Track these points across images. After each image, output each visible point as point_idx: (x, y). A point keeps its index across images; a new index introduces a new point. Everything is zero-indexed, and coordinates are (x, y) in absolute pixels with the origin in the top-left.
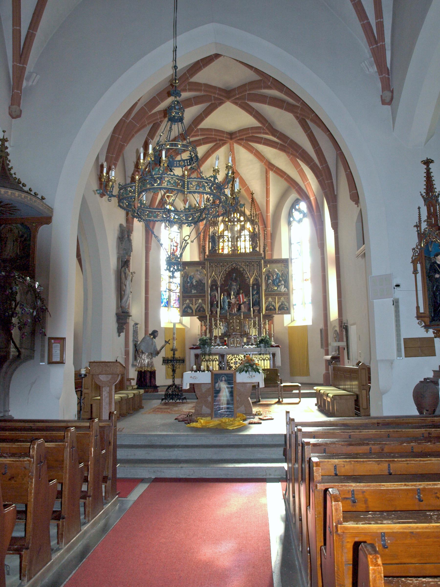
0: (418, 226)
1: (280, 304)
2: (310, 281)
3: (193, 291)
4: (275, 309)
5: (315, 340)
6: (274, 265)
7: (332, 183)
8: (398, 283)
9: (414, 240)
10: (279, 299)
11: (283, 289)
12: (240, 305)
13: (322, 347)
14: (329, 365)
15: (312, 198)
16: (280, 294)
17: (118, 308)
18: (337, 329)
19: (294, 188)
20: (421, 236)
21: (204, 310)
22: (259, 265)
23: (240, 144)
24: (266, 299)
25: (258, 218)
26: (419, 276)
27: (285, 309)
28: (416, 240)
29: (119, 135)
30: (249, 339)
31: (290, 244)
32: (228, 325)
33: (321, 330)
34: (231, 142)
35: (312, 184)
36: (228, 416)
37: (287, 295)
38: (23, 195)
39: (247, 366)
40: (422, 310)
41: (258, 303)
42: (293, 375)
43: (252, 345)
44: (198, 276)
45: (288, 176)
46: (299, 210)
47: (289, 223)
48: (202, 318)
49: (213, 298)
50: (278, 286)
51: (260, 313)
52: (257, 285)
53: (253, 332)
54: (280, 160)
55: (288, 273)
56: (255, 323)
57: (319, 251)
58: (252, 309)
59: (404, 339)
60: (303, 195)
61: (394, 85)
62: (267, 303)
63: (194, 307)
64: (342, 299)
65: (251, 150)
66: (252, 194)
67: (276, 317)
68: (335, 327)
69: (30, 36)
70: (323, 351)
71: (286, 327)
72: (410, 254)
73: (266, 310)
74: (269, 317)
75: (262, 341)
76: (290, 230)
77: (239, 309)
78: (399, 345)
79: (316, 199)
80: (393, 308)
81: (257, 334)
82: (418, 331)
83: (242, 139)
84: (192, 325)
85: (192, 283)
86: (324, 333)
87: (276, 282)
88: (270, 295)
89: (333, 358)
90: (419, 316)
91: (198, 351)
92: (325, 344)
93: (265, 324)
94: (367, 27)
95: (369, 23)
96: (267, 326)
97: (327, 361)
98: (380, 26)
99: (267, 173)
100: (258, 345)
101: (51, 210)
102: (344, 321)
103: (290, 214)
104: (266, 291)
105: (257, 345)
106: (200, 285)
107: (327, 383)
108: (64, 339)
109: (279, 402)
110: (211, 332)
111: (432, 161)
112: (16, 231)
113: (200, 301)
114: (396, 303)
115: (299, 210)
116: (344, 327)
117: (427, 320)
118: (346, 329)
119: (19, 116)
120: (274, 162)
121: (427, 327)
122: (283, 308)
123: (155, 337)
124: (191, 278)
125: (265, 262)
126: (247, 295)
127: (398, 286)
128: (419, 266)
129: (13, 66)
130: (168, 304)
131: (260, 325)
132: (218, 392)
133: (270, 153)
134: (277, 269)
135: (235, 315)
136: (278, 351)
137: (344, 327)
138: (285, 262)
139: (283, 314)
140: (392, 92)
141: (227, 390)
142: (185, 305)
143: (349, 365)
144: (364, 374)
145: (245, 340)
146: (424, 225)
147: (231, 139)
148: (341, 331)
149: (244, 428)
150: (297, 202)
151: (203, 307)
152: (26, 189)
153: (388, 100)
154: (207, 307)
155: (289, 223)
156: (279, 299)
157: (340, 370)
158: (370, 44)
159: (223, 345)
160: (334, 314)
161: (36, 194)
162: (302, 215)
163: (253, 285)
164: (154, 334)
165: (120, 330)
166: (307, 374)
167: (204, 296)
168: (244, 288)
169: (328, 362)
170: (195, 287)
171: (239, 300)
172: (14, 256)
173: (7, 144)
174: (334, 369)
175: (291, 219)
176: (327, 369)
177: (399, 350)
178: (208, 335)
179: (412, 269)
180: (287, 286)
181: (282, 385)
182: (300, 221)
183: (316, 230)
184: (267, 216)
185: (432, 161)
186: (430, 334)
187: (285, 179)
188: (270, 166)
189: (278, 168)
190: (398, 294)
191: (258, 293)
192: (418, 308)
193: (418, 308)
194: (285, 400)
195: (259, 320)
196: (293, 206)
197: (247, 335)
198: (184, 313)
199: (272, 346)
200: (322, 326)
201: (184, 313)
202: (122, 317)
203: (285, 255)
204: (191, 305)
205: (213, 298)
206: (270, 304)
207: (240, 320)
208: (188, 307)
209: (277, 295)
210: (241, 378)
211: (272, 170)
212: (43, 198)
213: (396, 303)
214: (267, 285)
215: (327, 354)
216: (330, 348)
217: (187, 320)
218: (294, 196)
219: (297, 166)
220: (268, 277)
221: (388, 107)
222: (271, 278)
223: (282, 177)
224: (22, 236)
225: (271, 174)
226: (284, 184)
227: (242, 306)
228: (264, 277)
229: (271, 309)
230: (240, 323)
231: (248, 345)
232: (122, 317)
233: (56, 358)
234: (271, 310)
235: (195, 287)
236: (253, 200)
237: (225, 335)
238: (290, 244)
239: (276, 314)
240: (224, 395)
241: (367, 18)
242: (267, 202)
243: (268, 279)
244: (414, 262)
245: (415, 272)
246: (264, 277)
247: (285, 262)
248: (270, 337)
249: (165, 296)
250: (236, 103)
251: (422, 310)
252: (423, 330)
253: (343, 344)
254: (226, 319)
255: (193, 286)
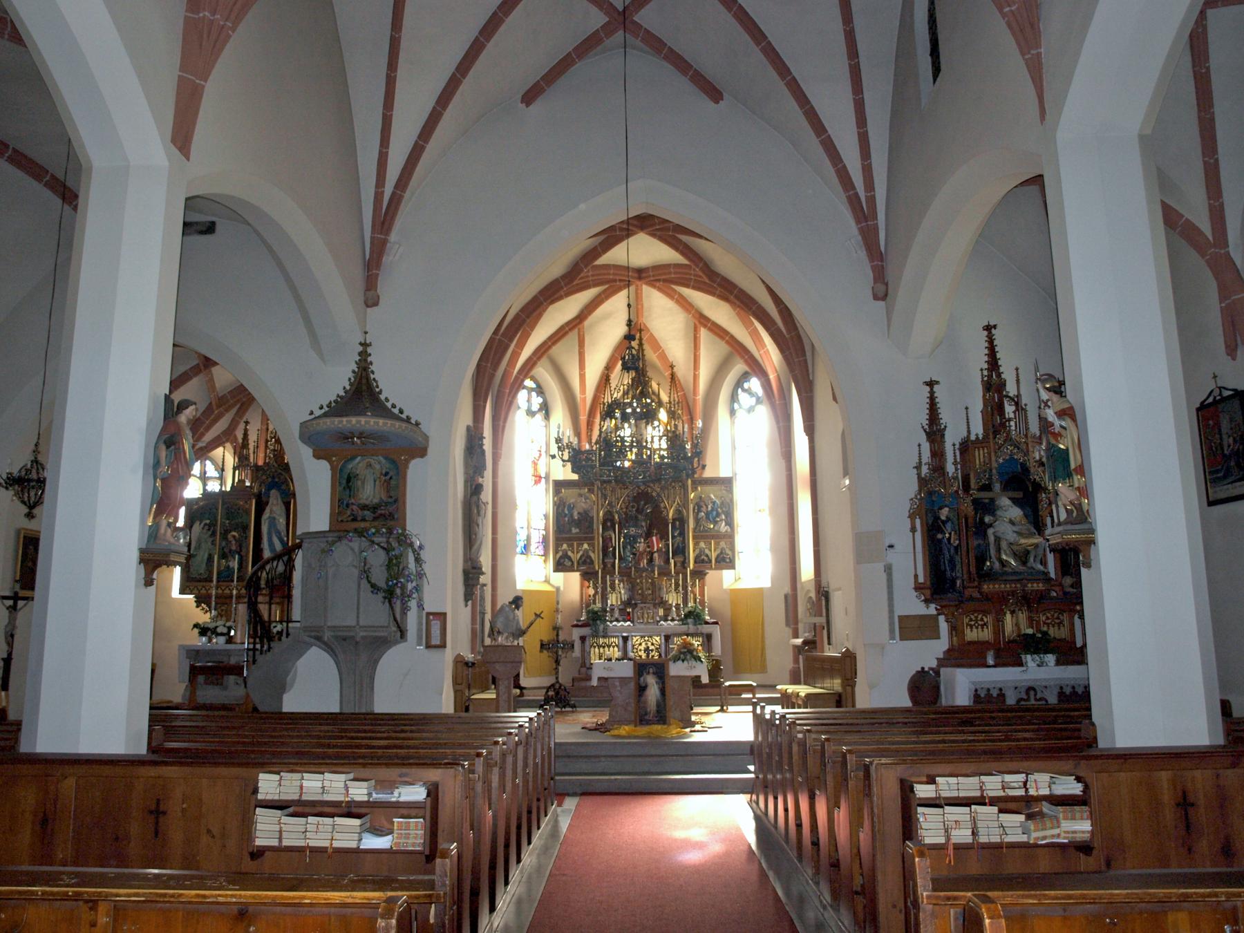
0: (918, 467)
1: (718, 552)
2: (767, 512)
3: (574, 530)
4: (710, 561)
5: (775, 613)
6: (708, 488)
7: (806, 361)
8: (893, 542)
9: (914, 486)
10: (717, 544)
11: (723, 528)
12: (652, 553)
13: (787, 624)
14: (799, 653)
15: (772, 377)
16: (718, 537)
17: (465, 561)
18: (813, 595)
19: (742, 357)
20: (922, 482)
21: (592, 562)
22: (684, 487)
23: (654, 287)
24: (696, 544)
25: (683, 408)
26: (918, 535)
27: (726, 561)
28: (916, 487)
29: (214, 14)
30: (668, 609)
31: (734, 448)
32: (632, 589)
33: (786, 596)
34: (639, 283)
35: (771, 355)
36: (658, 722)
37: (730, 537)
38: (398, 424)
39: (684, 653)
40: (921, 580)
41: (681, 551)
42: (737, 672)
43: (673, 620)
44: (582, 505)
45: (732, 337)
46: (748, 391)
47: (732, 412)
48: (588, 576)
49: (607, 541)
50: (715, 523)
51: (685, 568)
52: (681, 521)
53: (673, 599)
54: (720, 312)
55: (732, 500)
56: (677, 585)
57: (783, 464)
58: (672, 561)
59: (899, 617)
60: (756, 367)
61: (890, 276)
62: (697, 551)
63: (575, 557)
64: (821, 549)
65: (670, 294)
66: (672, 367)
67: (711, 575)
68: (808, 591)
69: (396, 200)
70: (788, 631)
71: (725, 591)
72: (906, 508)
73: (695, 562)
74: (699, 574)
75: (689, 614)
76: (733, 423)
77: (651, 560)
78: (891, 624)
79: (779, 378)
80: (884, 577)
81: (680, 602)
82: (914, 606)
83: (659, 280)
84: (570, 585)
85: (572, 516)
86: (791, 601)
87: (713, 517)
88: (703, 537)
89: (805, 643)
90: (918, 588)
91: (585, 631)
92: (792, 619)
93: (694, 585)
94: (854, 201)
95: (857, 194)
96: (697, 590)
97: (795, 647)
98: (872, 200)
99: (696, 330)
100: (684, 621)
101: (426, 438)
102: (824, 584)
103: (734, 398)
104: (694, 531)
105: (681, 620)
106: (585, 521)
107: (795, 680)
108: (445, 614)
109: (722, 710)
110: (604, 599)
111: (937, 383)
112: (378, 467)
113: (586, 546)
114: (888, 569)
115: (748, 391)
116: (823, 594)
117: (928, 592)
118: (827, 595)
119: (376, 304)
120: (707, 313)
121: (927, 601)
122: (724, 560)
123: (517, 607)
124: (571, 508)
125: (694, 482)
126: (664, 536)
127: (891, 546)
128: (918, 522)
129: (372, 238)
130: (526, 547)
131: (685, 588)
132: (642, 689)
133: (702, 300)
134: (713, 494)
135: (644, 570)
136: (716, 632)
137: (823, 594)
138: (727, 483)
139: (722, 569)
140: (887, 284)
141: (656, 687)
142: (560, 554)
143: (830, 652)
144: (846, 666)
145: (661, 612)
146: (925, 470)
147: (640, 278)
148: (819, 600)
149: (686, 735)
150: (745, 377)
151: (590, 557)
152: (404, 416)
153: (881, 294)
154: (596, 557)
155: (732, 412)
156: (717, 544)
157: (815, 659)
158: (858, 221)
159: (625, 621)
160: (807, 571)
161: (408, 420)
162: (754, 399)
163: (674, 520)
164: (517, 601)
165: (466, 600)
166: (763, 669)
167: (592, 538)
168: (657, 524)
169: (798, 650)
170: (578, 524)
171: (650, 546)
172: (376, 501)
173: (369, 350)
174: (806, 660)
175: (736, 406)
176: (796, 661)
177: (892, 631)
178: (599, 605)
179: (909, 526)
180: (730, 522)
181: (727, 684)
182: (751, 410)
183: (779, 428)
184: (695, 400)
185: (937, 383)
186: (932, 610)
187: (727, 342)
188: (702, 320)
189: (714, 324)
190: (891, 557)
191: (683, 534)
192: (916, 576)
193: (916, 576)
194: (731, 708)
195: (685, 579)
196: (739, 384)
197: (663, 603)
198: (560, 566)
199: (707, 623)
200: (787, 589)
201: (560, 566)
202: (471, 573)
203: (724, 473)
204: (570, 553)
205: (607, 541)
206: (702, 552)
207: (653, 578)
208: (565, 556)
209: (713, 537)
210: (677, 669)
211: (705, 326)
212: (417, 424)
213: (888, 569)
214: (697, 521)
215: (796, 636)
216: (801, 626)
217: (559, 579)
218: (739, 367)
219: (748, 325)
220: (698, 507)
221: (882, 303)
222: (704, 509)
223: (722, 338)
224: (386, 474)
225: (704, 333)
226: (723, 348)
227: (656, 555)
228: (691, 506)
229: (703, 561)
230: (653, 584)
231: (666, 620)
232: (471, 573)
233: (436, 640)
234: (703, 562)
235: (578, 524)
236: (673, 376)
237: (628, 603)
238: (734, 448)
239: (711, 568)
240: (653, 693)
241: (854, 188)
242: (696, 377)
243: (699, 511)
244: (912, 517)
245: (913, 530)
246: (691, 506)
247: (727, 483)
248: (704, 607)
249: (521, 537)
250: (653, 235)
251: (921, 580)
252: (923, 605)
253: (823, 620)
254: (629, 575)
255: (574, 521)
